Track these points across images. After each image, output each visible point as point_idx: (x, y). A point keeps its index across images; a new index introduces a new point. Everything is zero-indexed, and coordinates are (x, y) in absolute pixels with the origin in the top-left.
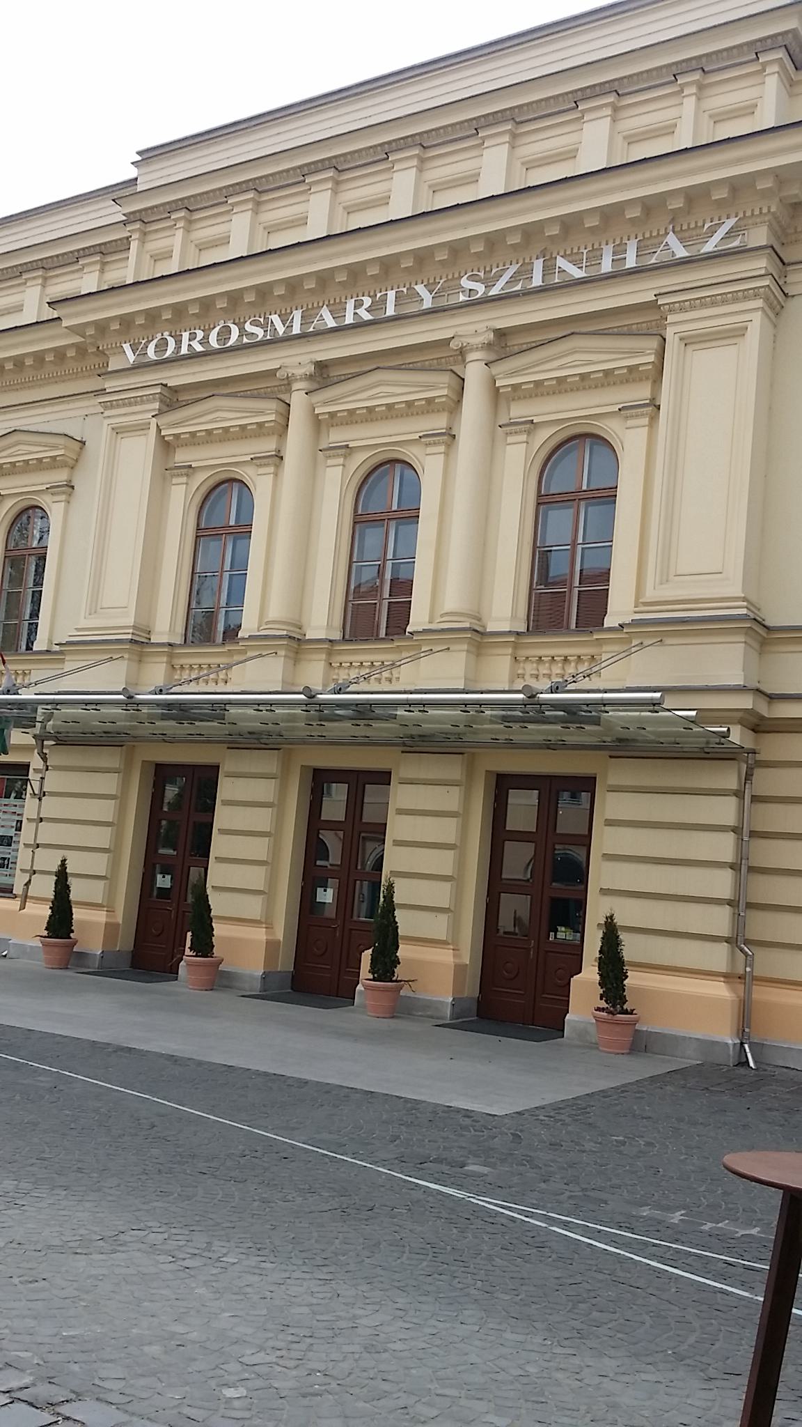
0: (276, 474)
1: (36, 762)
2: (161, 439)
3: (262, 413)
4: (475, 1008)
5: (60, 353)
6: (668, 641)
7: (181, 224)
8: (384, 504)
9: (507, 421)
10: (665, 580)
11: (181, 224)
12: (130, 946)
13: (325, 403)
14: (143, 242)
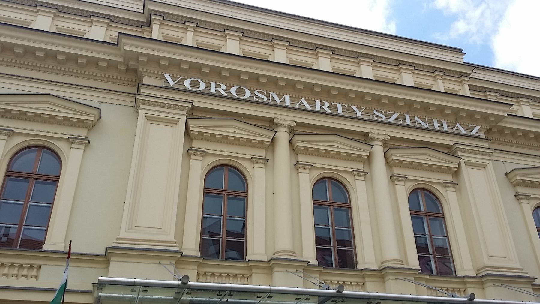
8: (332, 200)
13: (303, 142)
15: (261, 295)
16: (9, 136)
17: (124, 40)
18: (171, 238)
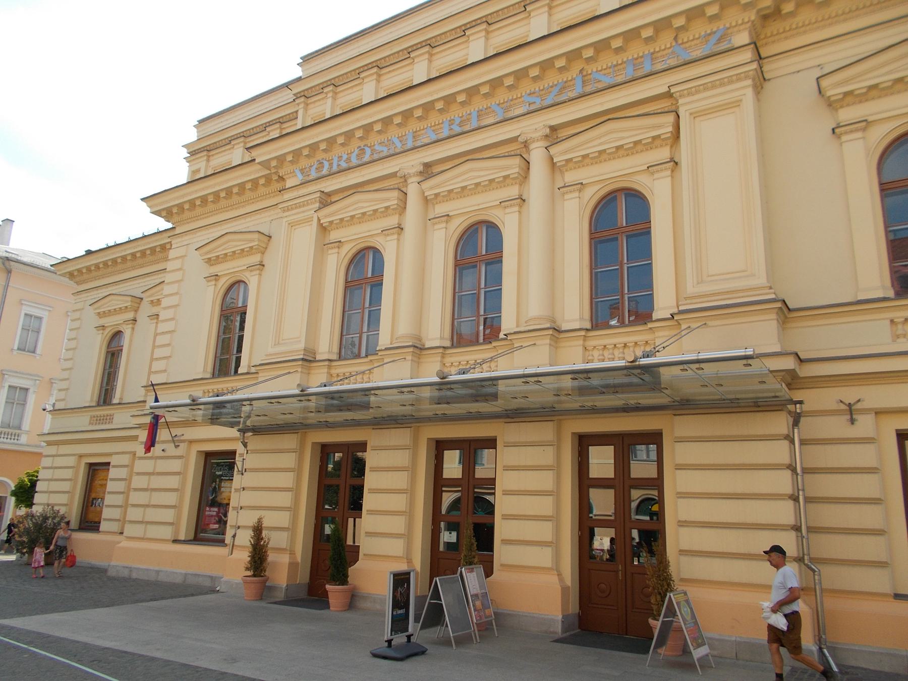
0: (398, 240)
1: (240, 449)
2: (320, 225)
3: (388, 200)
4: (577, 623)
5: (255, 182)
6: (710, 323)
7: (330, 95)
9: (562, 185)
10: (700, 282)
11: (330, 95)
12: (307, 579)
13: (431, 188)
14: (306, 110)
15: (452, 386)
16: (864, 129)
17: (255, 153)
18: (762, 280)
